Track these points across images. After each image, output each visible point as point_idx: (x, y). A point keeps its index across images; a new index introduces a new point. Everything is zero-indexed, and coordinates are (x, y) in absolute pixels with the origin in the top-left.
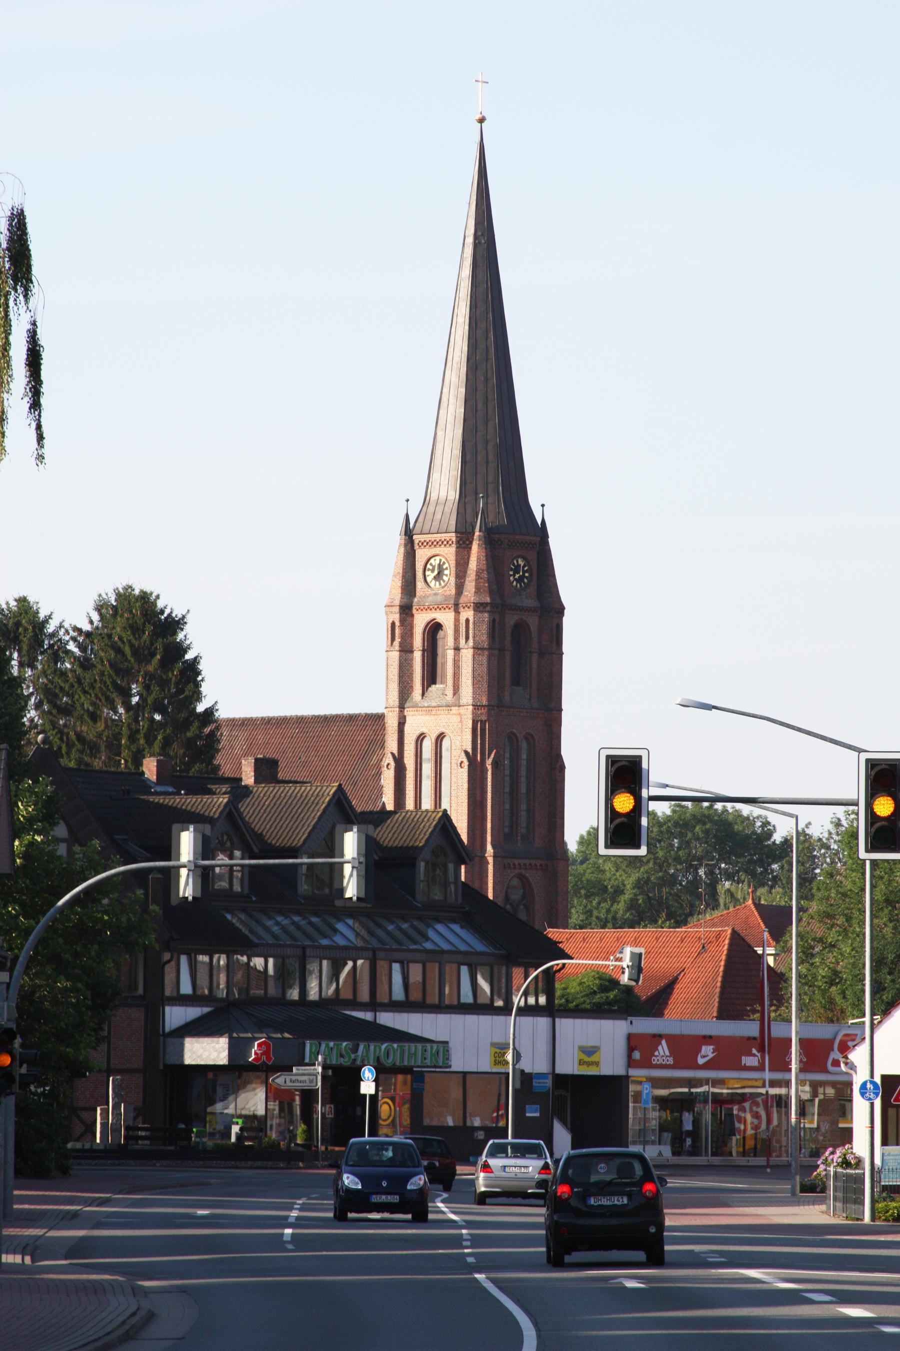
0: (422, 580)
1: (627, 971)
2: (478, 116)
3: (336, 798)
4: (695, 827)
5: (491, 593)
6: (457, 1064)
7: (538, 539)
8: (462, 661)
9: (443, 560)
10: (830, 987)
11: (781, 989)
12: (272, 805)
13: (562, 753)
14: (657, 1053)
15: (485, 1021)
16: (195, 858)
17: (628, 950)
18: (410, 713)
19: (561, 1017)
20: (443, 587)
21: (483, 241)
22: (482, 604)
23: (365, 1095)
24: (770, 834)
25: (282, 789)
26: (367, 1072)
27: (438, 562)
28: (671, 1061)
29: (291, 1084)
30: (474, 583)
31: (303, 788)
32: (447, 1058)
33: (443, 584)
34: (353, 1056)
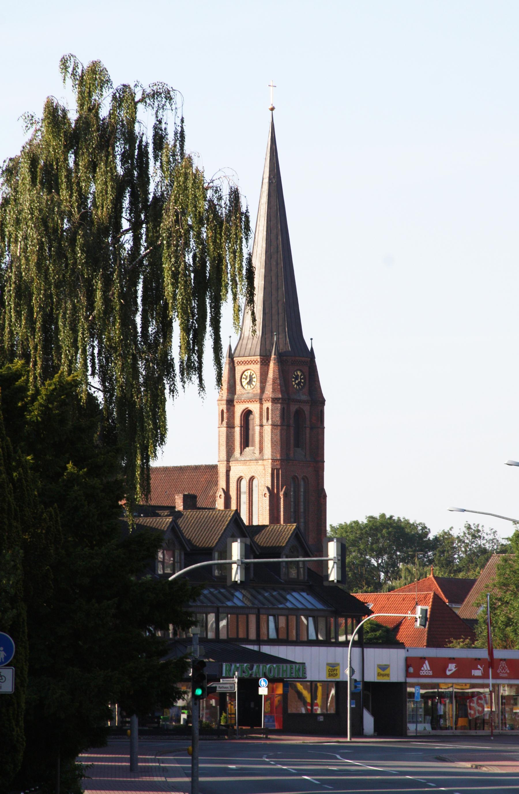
0: (240, 384)
1: (419, 620)
2: (270, 107)
3: (235, 517)
4: (382, 530)
5: (282, 392)
6: (311, 676)
7: (309, 359)
8: (265, 433)
9: (252, 372)
10: (506, 628)
11: (474, 629)
12: (196, 522)
13: (326, 487)
14: (422, 669)
15: (323, 650)
16: (241, 558)
18: (234, 465)
19: (367, 648)
20: (253, 389)
21: (274, 181)
22: (276, 399)
23: (262, 695)
24: (426, 534)
25: (201, 513)
28: (431, 673)
30: (271, 386)
31: (214, 512)
32: (305, 673)
33: (252, 387)
34: (250, 672)
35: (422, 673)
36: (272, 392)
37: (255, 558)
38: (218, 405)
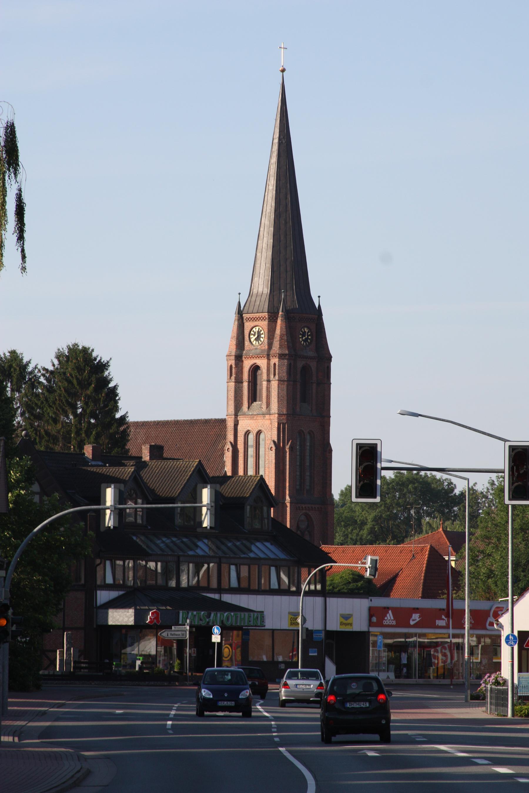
1: (368, 569)
2: (281, 68)
3: (198, 468)
4: (408, 485)
5: (289, 348)
6: (269, 625)
7: (317, 316)
8: (272, 389)
9: (261, 329)
10: (488, 580)
11: (459, 581)
12: (160, 472)
13: (331, 442)
14: (386, 618)
15: (285, 599)
16: (115, 504)
17: (369, 558)
19: (330, 597)
20: (260, 345)
21: (284, 142)
23: (215, 643)
24: (452, 490)
25: (166, 463)
26: (215, 629)
27: (257, 330)
28: (394, 623)
29: (171, 636)
30: (278, 342)
32: (263, 621)
34: (207, 620)
35: (385, 622)
36: (279, 348)
37: (147, 504)
38: (227, 360)
